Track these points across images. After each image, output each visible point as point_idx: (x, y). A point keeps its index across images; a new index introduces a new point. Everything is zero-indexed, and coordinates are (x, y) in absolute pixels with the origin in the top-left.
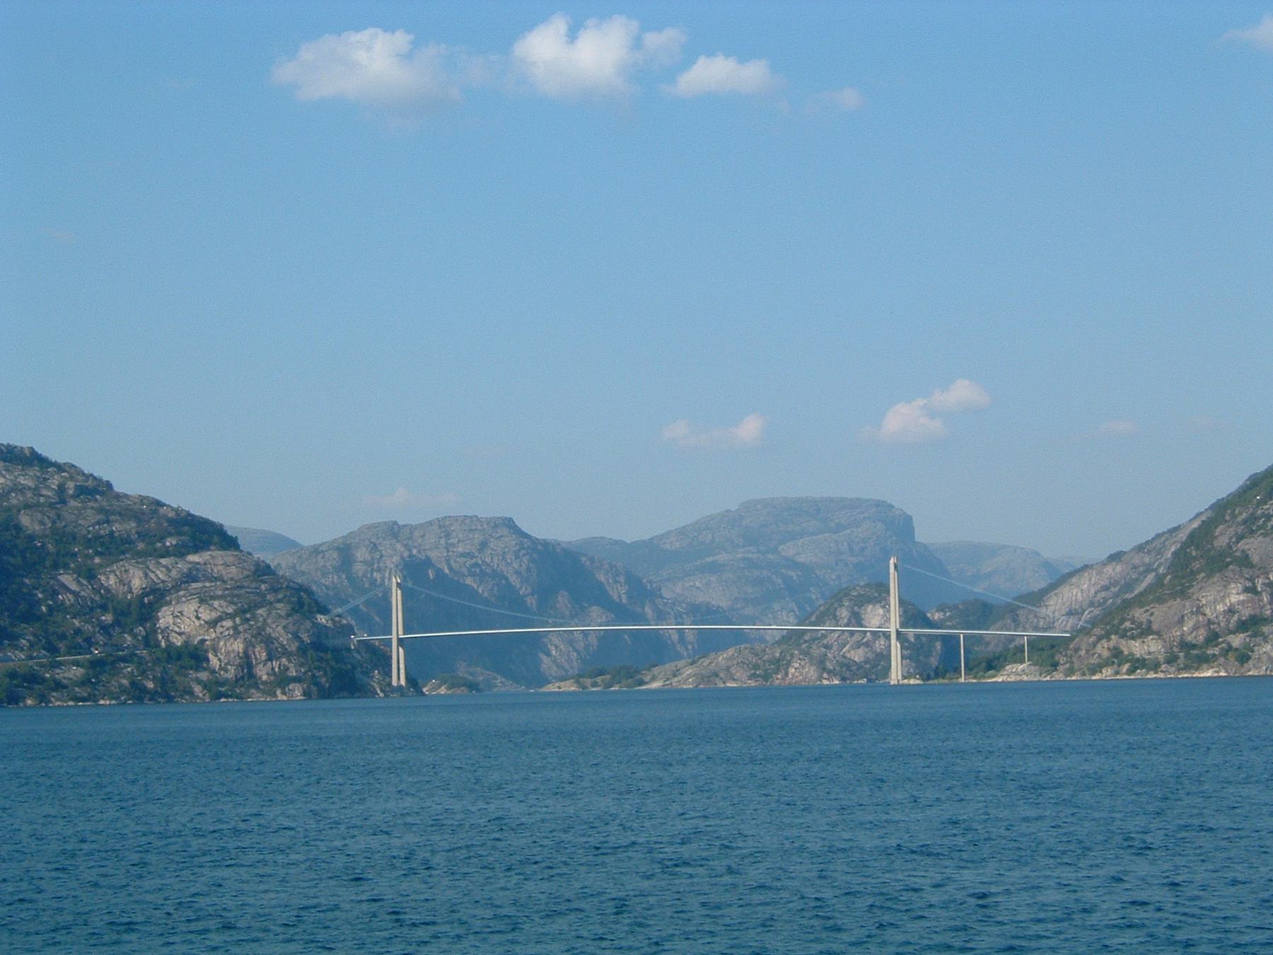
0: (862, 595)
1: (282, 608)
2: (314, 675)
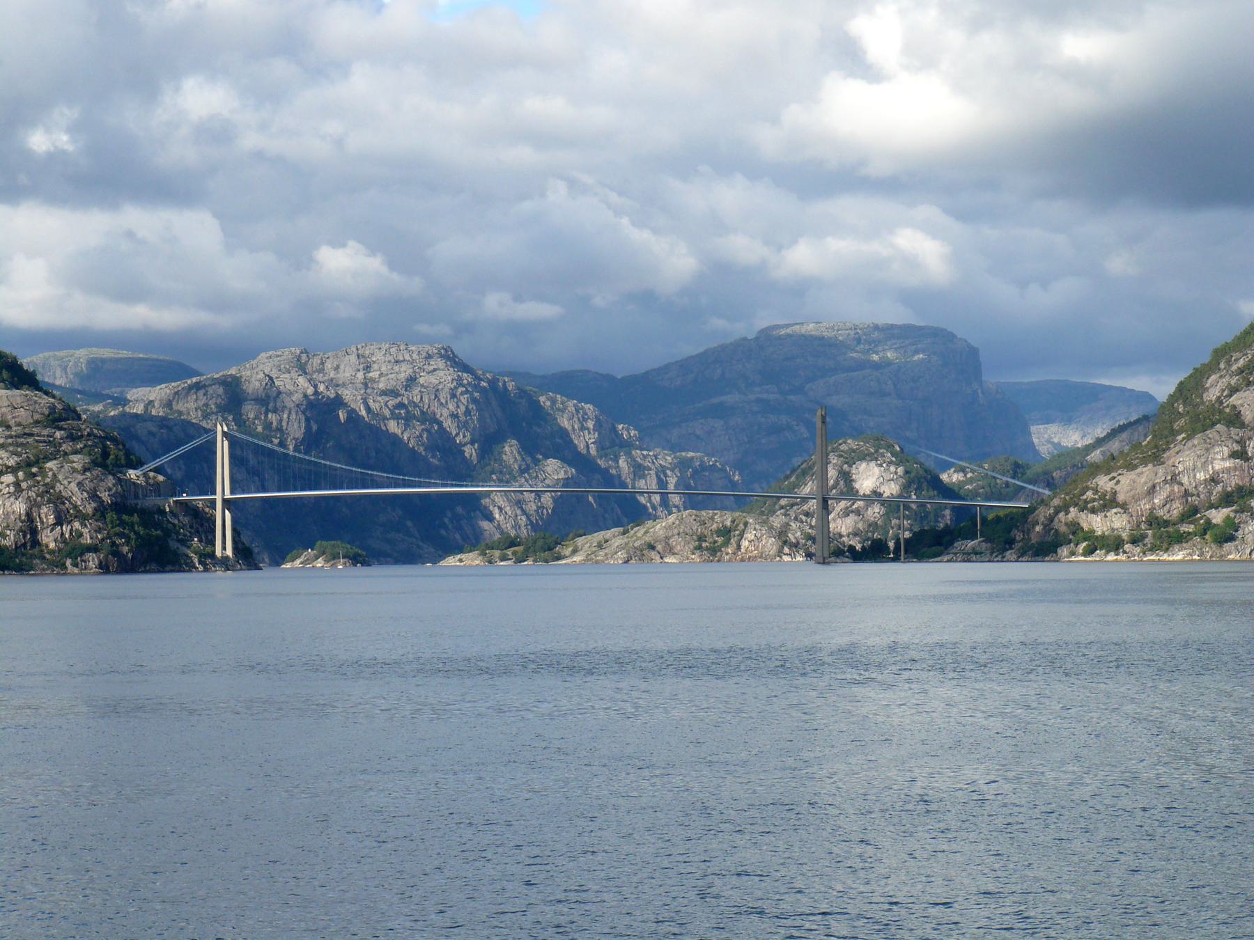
0: (854, 451)
1: (78, 461)
2: (113, 544)
